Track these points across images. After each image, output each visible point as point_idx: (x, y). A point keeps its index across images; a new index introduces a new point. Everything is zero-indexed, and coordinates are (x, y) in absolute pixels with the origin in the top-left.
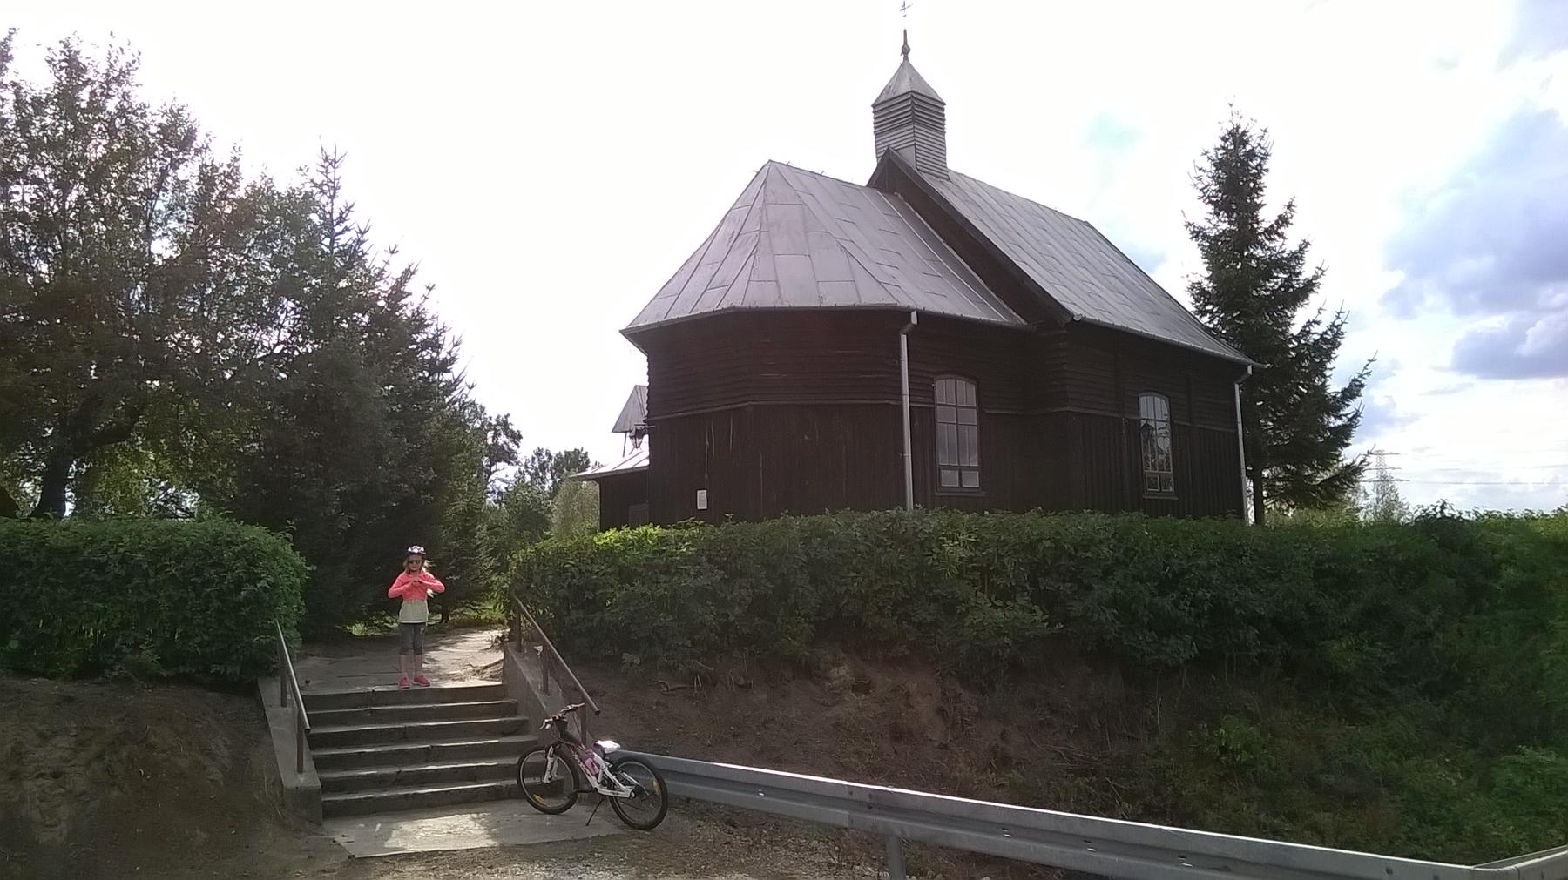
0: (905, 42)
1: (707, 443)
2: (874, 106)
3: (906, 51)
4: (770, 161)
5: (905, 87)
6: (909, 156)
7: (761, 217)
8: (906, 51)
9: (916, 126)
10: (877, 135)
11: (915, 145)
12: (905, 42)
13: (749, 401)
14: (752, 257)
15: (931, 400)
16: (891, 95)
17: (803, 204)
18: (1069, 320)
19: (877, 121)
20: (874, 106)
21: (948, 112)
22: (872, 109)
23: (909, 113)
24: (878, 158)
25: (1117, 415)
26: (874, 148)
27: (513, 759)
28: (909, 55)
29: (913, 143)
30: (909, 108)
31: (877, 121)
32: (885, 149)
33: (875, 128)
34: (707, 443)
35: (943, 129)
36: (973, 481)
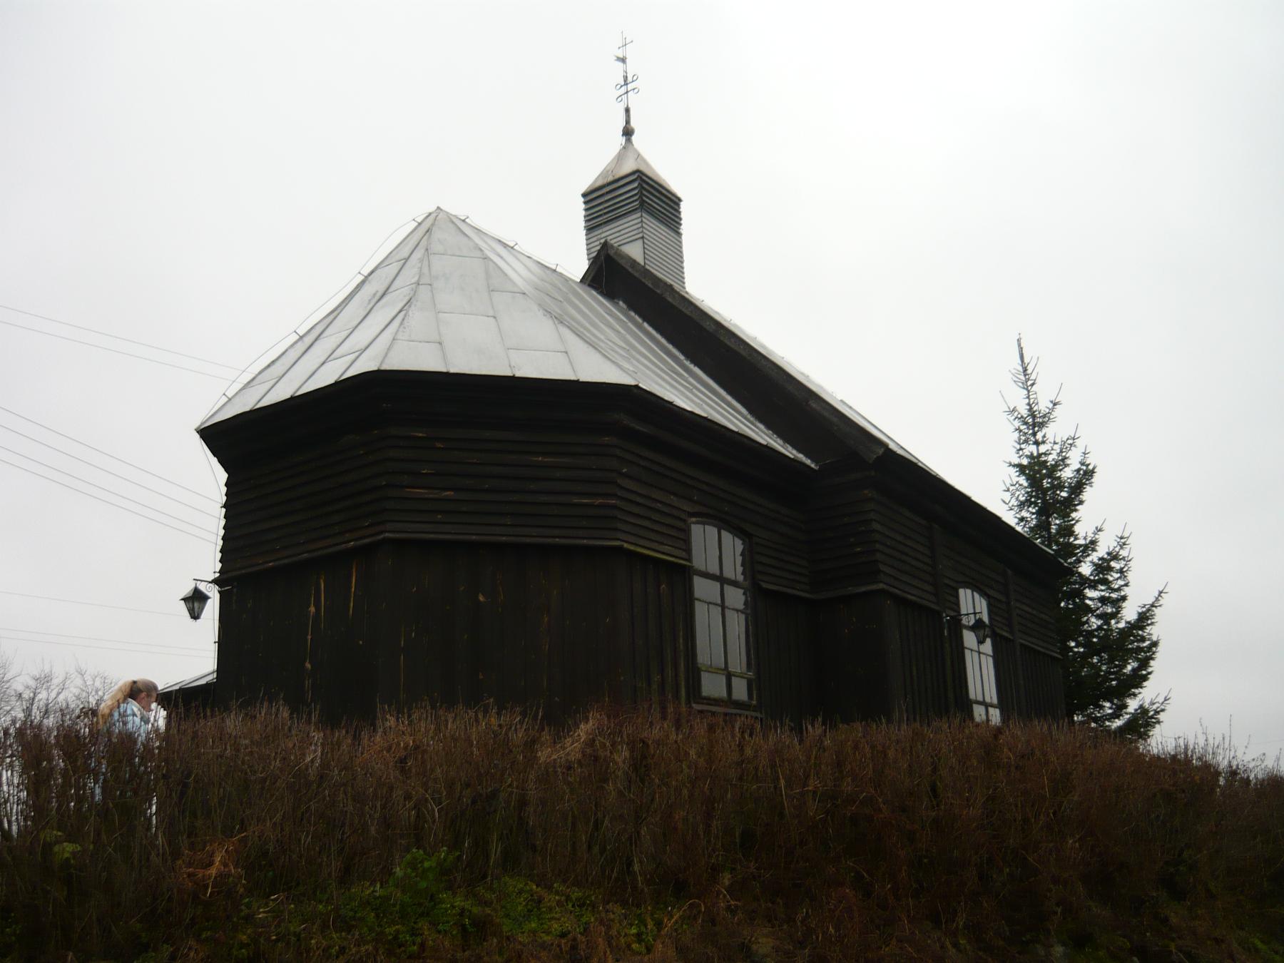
0: (628, 122)
1: (312, 609)
2: (584, 195)
3: (628, 132)
4: (438, 208)
5: (628, 167)
6: (634, 251)
7: (421, 268)
8: (628, 132)
9: (643, 214)
10: (590, 229)
11: (643, 237)
12: (628, 122)
13: (386, 532)
14: (403, 313)
15: (684, 554)
16: (610, 179)
17: (486, 258)
18: (881, 451)
19: (590, 241)
20: (584, 195)
21: (684, 208)
22: (582, 200)
23: (635, 198)
24: (589, 259)
25: (937, 608)
26: (585, 247)
27: (971, 660)
28: (634, 138)
29: (641, 235)
30: (636, 192)
31: (590, 241)
32: (602, 241)
33: (586, 221)
34: (312, 609)
35: (679, 229)
36: (740, 691)
